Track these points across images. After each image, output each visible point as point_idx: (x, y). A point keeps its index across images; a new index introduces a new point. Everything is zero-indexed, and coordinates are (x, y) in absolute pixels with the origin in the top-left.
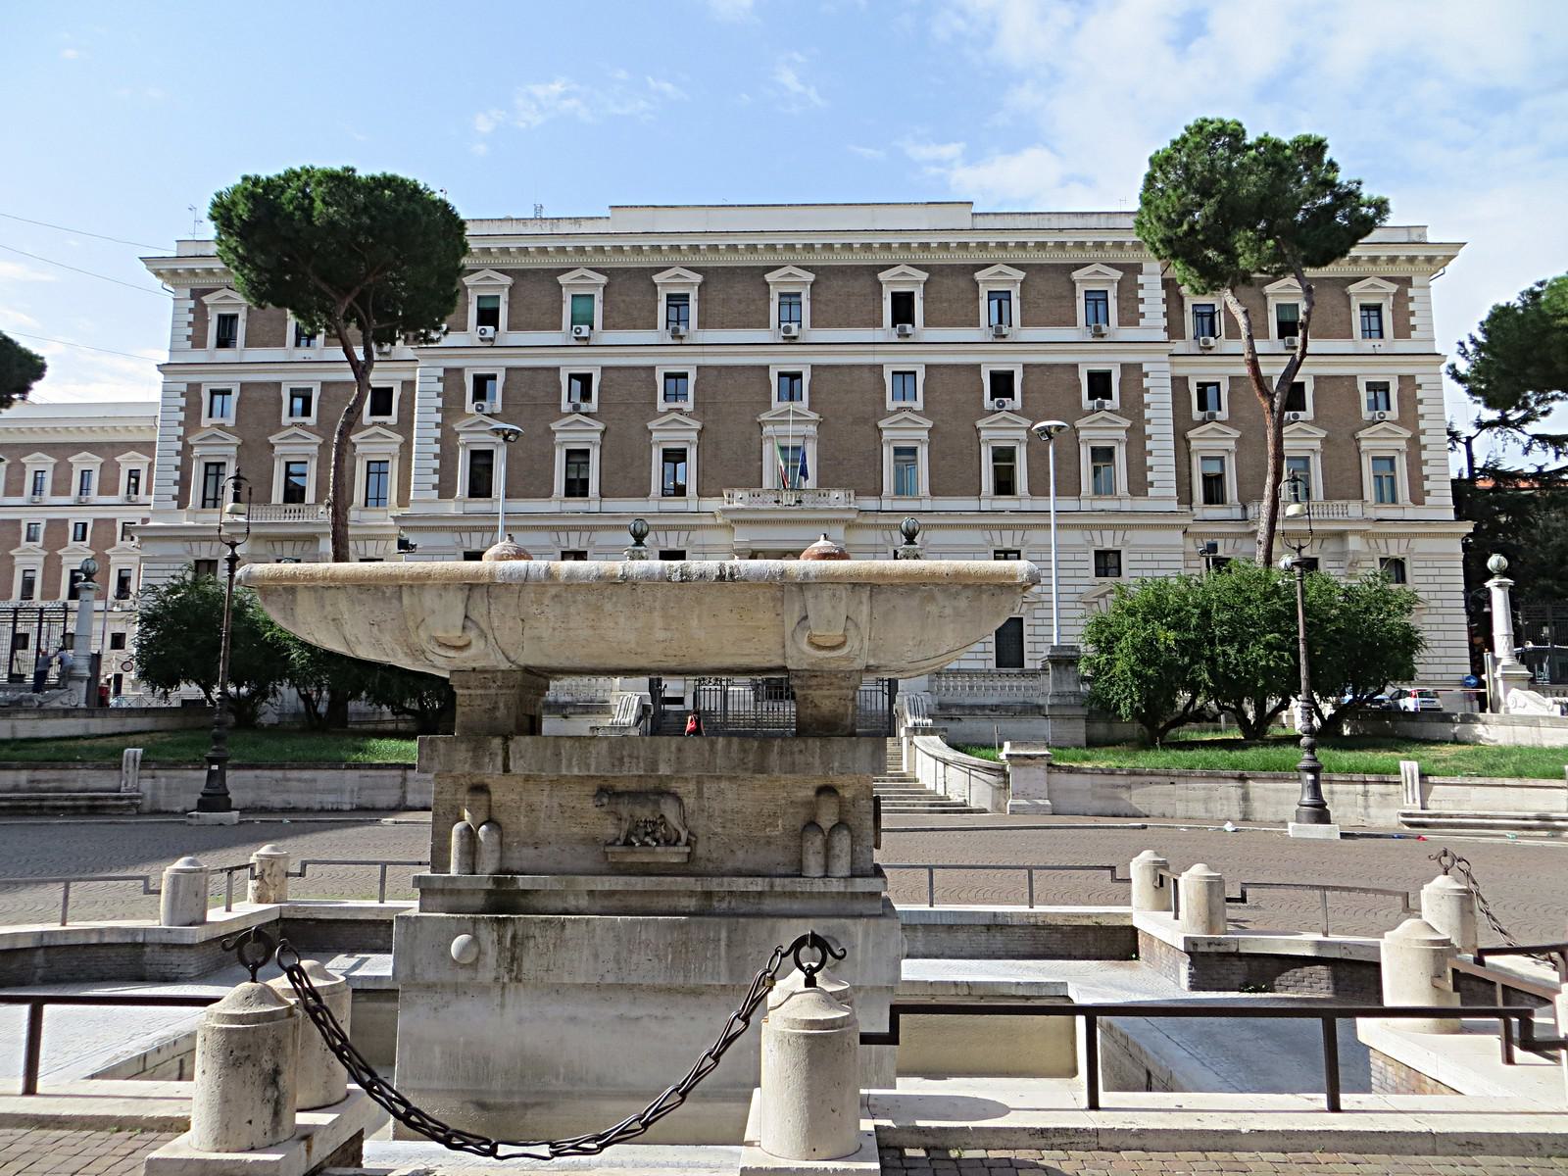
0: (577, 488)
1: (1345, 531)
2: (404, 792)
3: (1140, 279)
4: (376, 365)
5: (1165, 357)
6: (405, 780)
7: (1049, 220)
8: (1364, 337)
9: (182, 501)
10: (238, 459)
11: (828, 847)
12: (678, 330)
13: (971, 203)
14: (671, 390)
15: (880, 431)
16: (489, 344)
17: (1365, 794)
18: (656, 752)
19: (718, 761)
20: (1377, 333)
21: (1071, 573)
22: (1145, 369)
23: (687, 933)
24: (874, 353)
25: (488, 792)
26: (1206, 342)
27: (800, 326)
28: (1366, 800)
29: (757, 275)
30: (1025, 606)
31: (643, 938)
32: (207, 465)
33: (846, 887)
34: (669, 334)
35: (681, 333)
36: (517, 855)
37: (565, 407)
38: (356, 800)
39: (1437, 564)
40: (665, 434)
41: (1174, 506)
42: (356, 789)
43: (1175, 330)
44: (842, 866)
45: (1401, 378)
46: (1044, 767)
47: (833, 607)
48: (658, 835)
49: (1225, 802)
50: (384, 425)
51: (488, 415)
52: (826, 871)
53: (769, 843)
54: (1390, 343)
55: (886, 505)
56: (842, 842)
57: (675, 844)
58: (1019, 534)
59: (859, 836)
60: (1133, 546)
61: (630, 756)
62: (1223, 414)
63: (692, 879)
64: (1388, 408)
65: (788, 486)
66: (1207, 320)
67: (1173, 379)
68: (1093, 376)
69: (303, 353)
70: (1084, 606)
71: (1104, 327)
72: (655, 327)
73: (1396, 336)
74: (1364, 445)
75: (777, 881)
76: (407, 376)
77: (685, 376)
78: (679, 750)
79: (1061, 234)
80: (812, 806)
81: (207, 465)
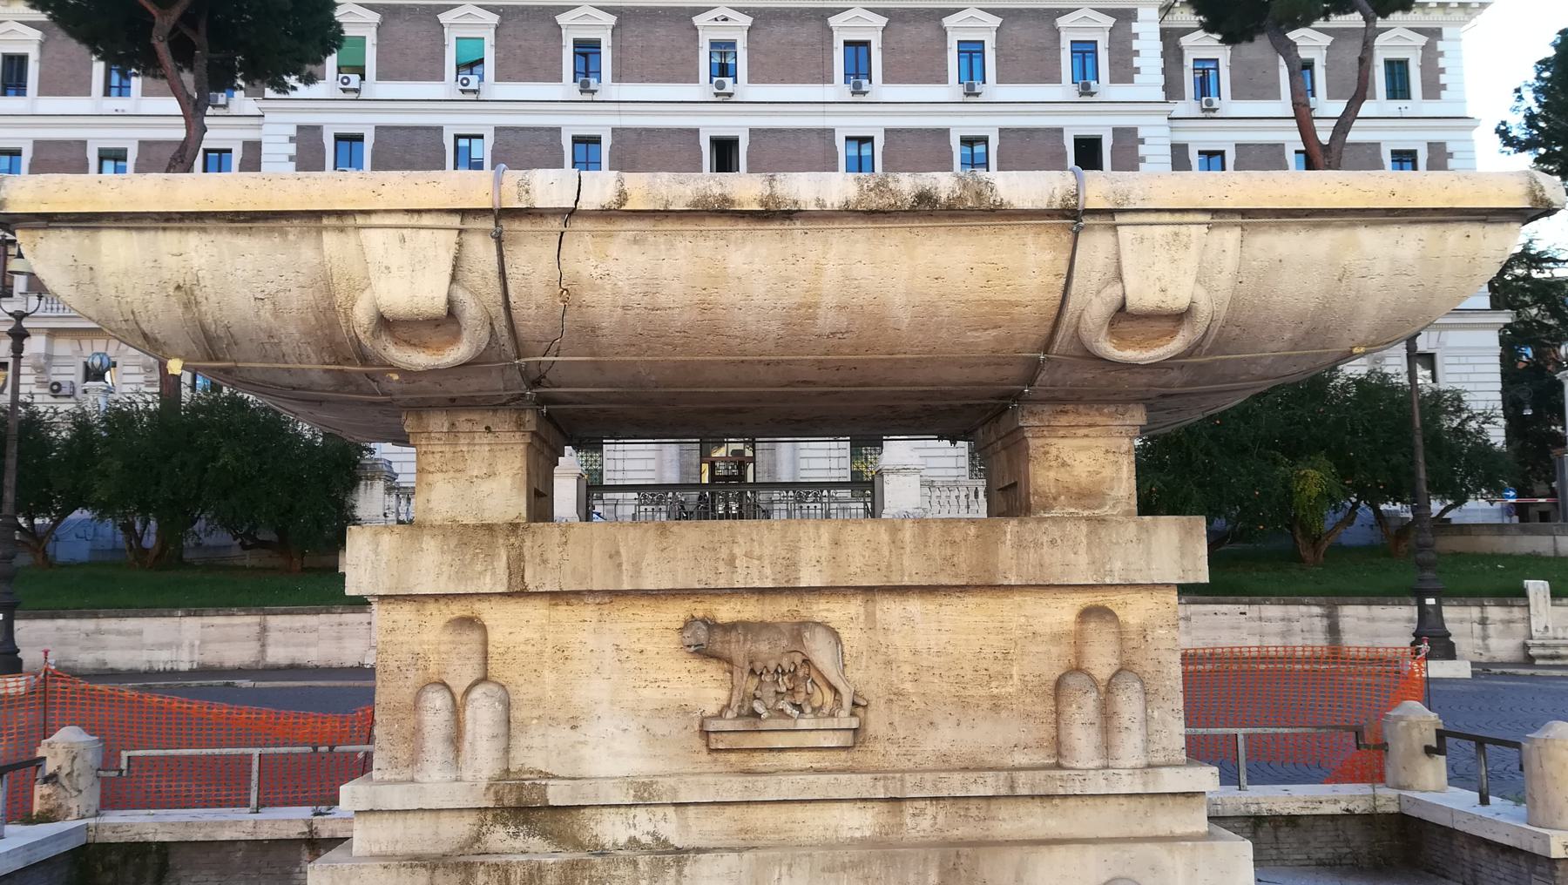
2: (263, 646)
3: (1135, 27)
6: (264, 629)
11: (1107, 718)
12: (589, 83)
14: (581, 157)
17: (1483, 622)
18: (794, 548)
19: (906, 562)
24: (824, 113)
25: (483, 628)
26: (1209, 103)
28: (1484, 630)
33: (1145, 784)
34: (577, 87)
35: (592, 88)
36: (537, 742)
38: (197, 657)
39: (1471, 360)
42: (197, 643)
43: (1172, 90)
47: (1173, 261)
48: (800, 699)
49: (1307, 635)
53: (996, 708)
54: (1417, 104)
57: (832, 715)
61: (749, 555)
63: (867, 778)
67: (1173, 146)
68: (1079, 142)
69: (115, 103)
71: (1093, 83)
73: (1425, 97)
75: (1022, 777)
76: (251, 135)
80: (1078, 642)
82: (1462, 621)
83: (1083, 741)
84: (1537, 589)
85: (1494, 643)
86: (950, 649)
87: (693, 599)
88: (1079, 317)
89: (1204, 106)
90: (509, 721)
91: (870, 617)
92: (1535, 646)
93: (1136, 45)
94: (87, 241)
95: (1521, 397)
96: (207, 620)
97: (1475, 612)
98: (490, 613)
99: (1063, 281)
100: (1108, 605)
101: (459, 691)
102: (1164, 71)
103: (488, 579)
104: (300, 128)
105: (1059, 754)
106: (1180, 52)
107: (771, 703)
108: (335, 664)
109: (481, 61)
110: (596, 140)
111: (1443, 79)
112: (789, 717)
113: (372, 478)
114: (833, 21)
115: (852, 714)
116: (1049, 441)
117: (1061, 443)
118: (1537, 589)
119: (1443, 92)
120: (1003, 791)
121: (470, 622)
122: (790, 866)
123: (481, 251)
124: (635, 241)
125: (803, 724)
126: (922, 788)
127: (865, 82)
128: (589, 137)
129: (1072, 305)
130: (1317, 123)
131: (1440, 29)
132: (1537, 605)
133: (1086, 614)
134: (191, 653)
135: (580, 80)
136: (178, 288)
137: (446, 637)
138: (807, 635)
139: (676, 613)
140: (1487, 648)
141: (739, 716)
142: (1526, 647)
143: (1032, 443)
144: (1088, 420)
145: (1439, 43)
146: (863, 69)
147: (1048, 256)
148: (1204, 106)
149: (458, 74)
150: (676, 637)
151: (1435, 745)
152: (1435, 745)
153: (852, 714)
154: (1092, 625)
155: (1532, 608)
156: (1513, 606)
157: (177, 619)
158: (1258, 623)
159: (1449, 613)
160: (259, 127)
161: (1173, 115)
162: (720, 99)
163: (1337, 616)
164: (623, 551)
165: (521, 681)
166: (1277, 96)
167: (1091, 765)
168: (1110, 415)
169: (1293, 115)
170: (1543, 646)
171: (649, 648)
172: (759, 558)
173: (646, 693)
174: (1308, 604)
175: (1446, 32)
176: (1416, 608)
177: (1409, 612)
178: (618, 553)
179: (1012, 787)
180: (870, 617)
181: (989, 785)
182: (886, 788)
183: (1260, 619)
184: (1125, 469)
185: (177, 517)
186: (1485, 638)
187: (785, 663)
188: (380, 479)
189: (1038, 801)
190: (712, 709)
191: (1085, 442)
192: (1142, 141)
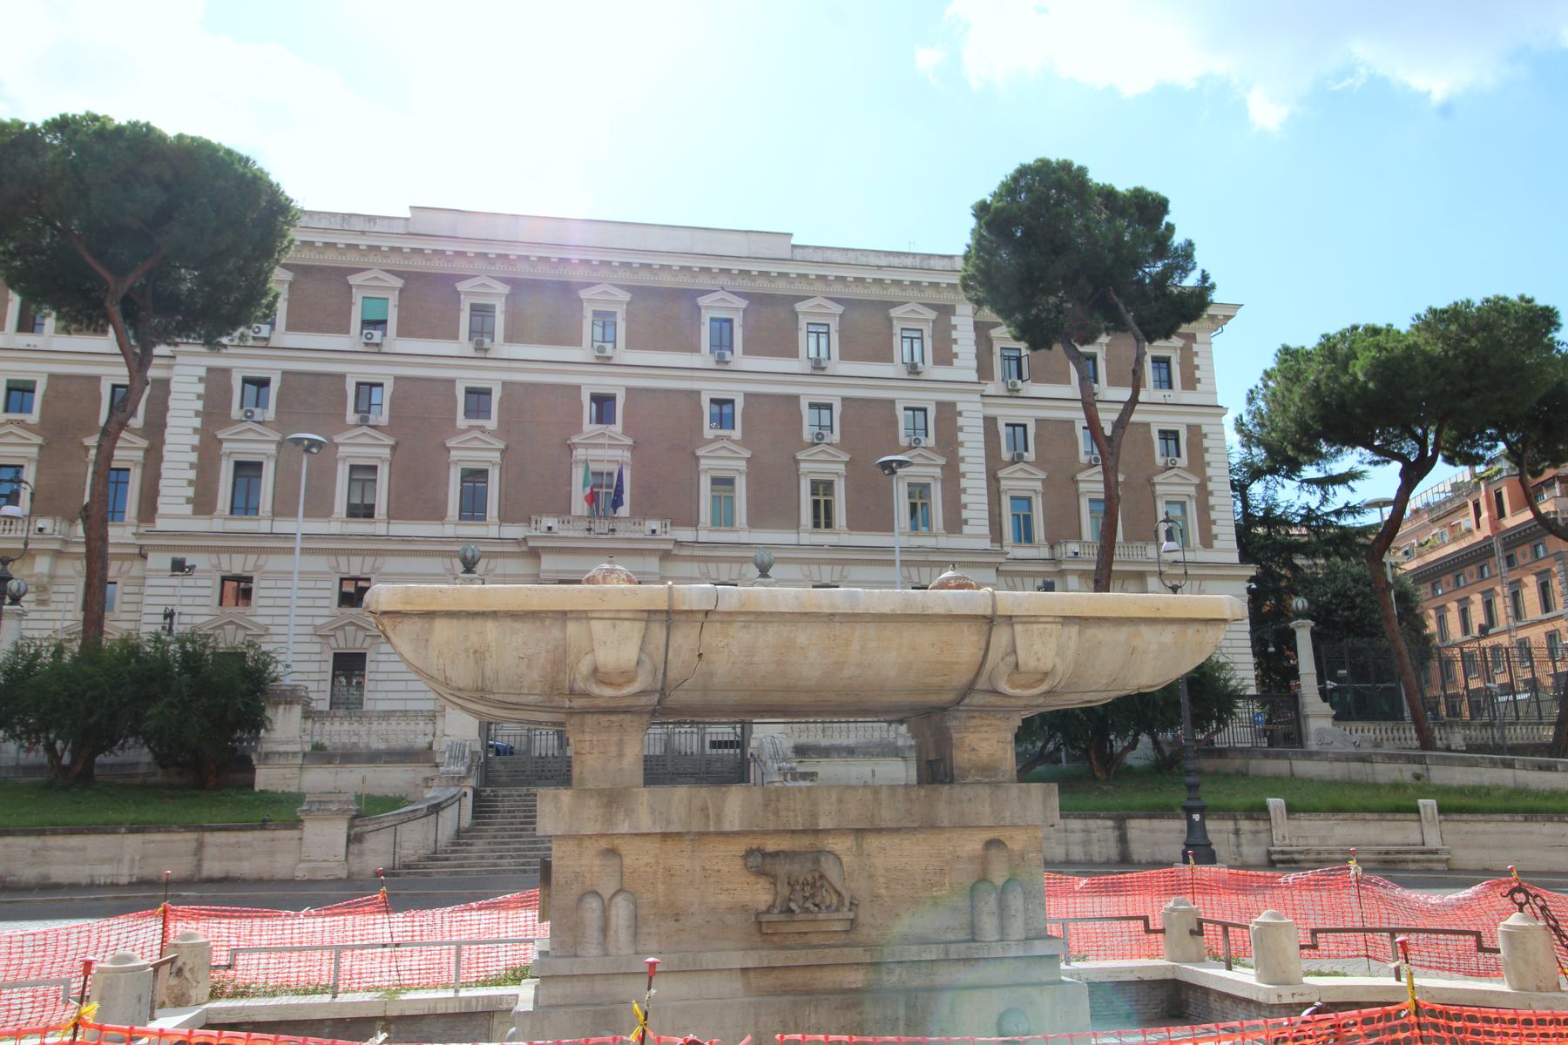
0: (361, 511)
1: (1144, 572)
3: (954, 320)
4: (155, 361)
5: (977, 398)
6: (201, 845)
7: (867, 256)
8: (1155, 387)
10: (41, 464)
11: (1002, 908)
13: (791, 235)
16: (263, 344)
17: (1237, 832)
20: (1166, 384)
21: (319, 602)
23: (861, 1013)
24: (691, 378)
25: (620, 856)
26: (1014, 384)
27: (615, 347)
29: (690, 296)
30: (369, 640)
31: (813, 1021)
35: (485, 346)
37: (236, 412)
38: (136, 871)
40: (813, 466)
41: (986, 544)
42: (137, 857)
43: (984, 371)
44: (1017, 928)
45: (1189, 427)
47: (1043, 643)
49: (1103, 844)
50: (21, 423)
51: (259, 423)
52: (973, 933)
53: (935, 904)
54: (1178, 394)
55: (703, 536)
56: (1016, 901)
57: (837, 910)
58: (736, 567)
60: (382, 574)
62: (1030, 455)
64: (1178, 455)
65: (601, 513)
66: (1014, 364)
67: (986, 419)
70: (319, 639)
72: (892, 361)
74: (1159, 489)
75: (953, 947)
78: (840, 801)
79: (364, 237)
80: (984, 862)
82: (1220, 831)
83: (989, 926)
85: (1245, 849)
86: (908, 867)
87: (750, 836)
88: (991, 673)
90: (636, 917)
91: (860, 846)
92: (1276, 852)
93: (955, 335)
94: (426, 625)
95: (1266, 637)
97: (1230, 825)
98: (625, 847)
99: (982, 652)
100: (1001, 838)
101: (607, 897)
102: (977, 356)
103: (626, 825)
104: (210, 370)
105: (973, 933)
106: (989, 341)
107: (801, 903)
108: (266, 876)
109: (384, 322)
110: (487, 392)
111: (1198, 374)
112: (812, 912)
113: (291, 703)
114: (703, 301)
115: (850, 910)
116: (965, 735)
117: (971, 736)
119: (1198, 385)
120: (942, 957)
121: (612, 852)
122: (816, 1007)
123: (658, 632)
124: (745, 627)
125: (821, 916)
127: (728, 353)
128: (481, 389)
129: (989, 665)
130: (1098, 405)
131: (1195, 335)
132: (1276, 819)
134: (132, 867)
135: (475, 339)
136: (476, 652)
137: (597, 862)
138: (823, 859)
139: (740, 846)
140: (1240, 854)
141: (781, 912)
142: (1269, 853)
143: (955, 736)
144: (988, 722)
145: (1194, 345)
146: (726, 341)
147: (975, 638)
149: (362, 329)
150: (740, 862)
151: (1196, 929)
152: (1196, 929)
153: (850, 910)
154: (993, 851)
155: (1273, 822)
156: (1258, 819)
157: (119, 836)
158: (1063, 835)
159: (1210, 825)
160: (170, 367)
161: (985, 393)
162: (599, 361)
163: (1126, 828)
164: (710, 806)
165: (643, 890)
166: (1068, 382)
167: (993, 939)
168: (1001, 719)
169: (1080, 397)
170: (1283, 852)
171: (724, 868)
172: (794, 811)
173: (722, 897)
175: (1199, 337)
176: (1185, 822)
177: (1181, 824)
178: (707, 808)
179: (947, 954)
180: (860, 846)
181: (932, 953)
182: (872, 956)
183: (1066, 831)
184: (1009, 752)
185: (94, 739)
186: (1238, 846)
187: (810, 880)
188: (298, 704)
189: (961, 963)
190: (763, 907)
191: (986, 735)
192: (960, 414)
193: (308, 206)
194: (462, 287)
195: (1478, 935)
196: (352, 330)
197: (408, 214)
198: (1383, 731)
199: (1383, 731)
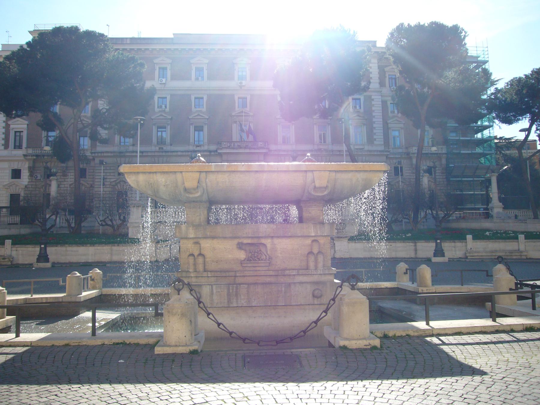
9: (6, 146)
15: (9, 125)
22: (373, 97)
25: (200, 244)
32: (16, 132)
46: (347, 241)
59: (326, 256)
66: (393, 81)
67: (382, 101)
77: (166, 98)
81: (16, 132)
84: (469, 237)
89: (392, 90)
96: (96, 248)
112: (257, 260)
115: (269, 260)
118: (469, 237)
126: (282, 273)
133: (313, 241)
137: (193, 246)
148: (392, 90)
157: (87, 247)
174: (409, 242)
190: (243, 259)
193: (110, 36)
194: (156, 61)
195: (487, 271)
196: (156, 79)
197: (172, 36)
198: (521, 213)
199: (521, 213)
